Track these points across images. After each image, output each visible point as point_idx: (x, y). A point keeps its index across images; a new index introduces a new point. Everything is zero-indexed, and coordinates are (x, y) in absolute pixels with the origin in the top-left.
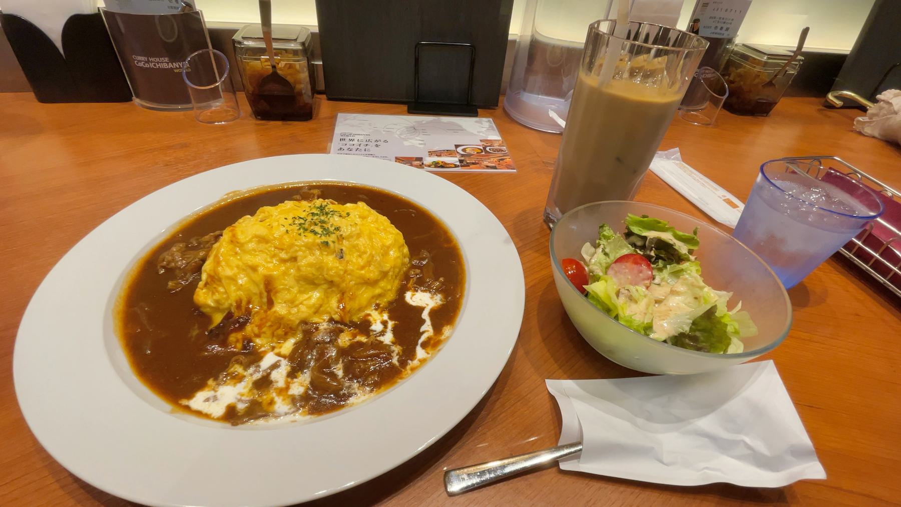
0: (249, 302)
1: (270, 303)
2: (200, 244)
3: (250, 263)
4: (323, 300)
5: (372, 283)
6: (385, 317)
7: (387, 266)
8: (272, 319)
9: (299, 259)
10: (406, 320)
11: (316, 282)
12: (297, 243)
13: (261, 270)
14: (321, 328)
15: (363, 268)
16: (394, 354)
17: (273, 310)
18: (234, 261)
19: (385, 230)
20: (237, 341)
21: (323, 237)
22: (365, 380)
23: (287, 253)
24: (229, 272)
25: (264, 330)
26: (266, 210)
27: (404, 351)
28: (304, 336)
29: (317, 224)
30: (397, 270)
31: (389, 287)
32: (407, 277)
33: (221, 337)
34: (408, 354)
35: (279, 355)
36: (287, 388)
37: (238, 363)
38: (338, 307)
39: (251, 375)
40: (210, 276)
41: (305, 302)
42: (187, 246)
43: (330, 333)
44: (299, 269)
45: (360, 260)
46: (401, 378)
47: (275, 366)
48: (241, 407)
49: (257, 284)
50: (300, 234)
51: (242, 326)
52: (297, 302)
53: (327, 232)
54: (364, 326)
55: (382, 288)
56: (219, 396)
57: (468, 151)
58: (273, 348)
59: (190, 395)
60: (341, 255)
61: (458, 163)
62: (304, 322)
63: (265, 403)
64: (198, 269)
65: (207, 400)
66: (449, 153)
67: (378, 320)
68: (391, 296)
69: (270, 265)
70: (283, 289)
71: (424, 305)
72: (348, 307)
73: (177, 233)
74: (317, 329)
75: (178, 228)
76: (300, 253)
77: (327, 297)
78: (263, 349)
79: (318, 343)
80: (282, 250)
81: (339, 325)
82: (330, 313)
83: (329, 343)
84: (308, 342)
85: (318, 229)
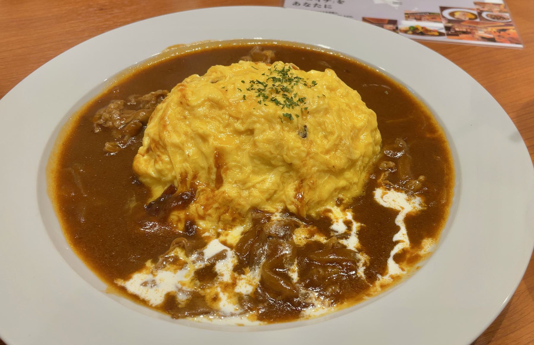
0: (195, 177)
1: (219, 181)
2: (139, 103)
3: (201, 131)
4: (279, 186)
5: (334, 172)
6: (349, 216)
7: (357, 154)
8: (220, 200)
9: (256, 132)
10: (377, 226)
11: (273, 162)
12: (255, 113)
13: (211, 140)
14: (274, 218)
15: (327, 152)
16: (360, 264)
17: (222, 189)
18: (183, 127)
19: (356, 107)
20: (179, 220)
21: (286, 109)
22: (325, 290)
23: (243, 123)
24: (175, 139)
25: (210, 211)
26: (218, 70)
27: (372, 262)
28: (254, 225)
29: (278, 92)
30: (367, 160)
31: (356, 180)
32: (376, 170)
33: (162, 214)
34: (377, 267)
35: (224, 243)
36: (234, 284)
37: (179, 246)
38: (295, 197)
39: (194, 262)
40: (153, 140)
41: (258, 186)
42: (125, 105)
43: (285, 225)
44: (255, 144)
45: (325, 142)
46: (369, 295)
47: (221, 256)
48: (182, 298)
49: (206, 158)
50: (260, 102)
51: (186, 204)
52: (250, 184)
53: (290, 103)
54: (323, 224)
55: (347, 180)
56: (158, 282)
57: (457, 15)
58: (218, 235)
59: (126, 276)
60: (304, 134)
61: (444, 31)
62: (255, 209)
63: (208, 297)
64: (139, 131)
65: (145, 284)
66: (433, 17)
67: (340, 219)
68: (356, 191)
69: (222, 136)
70: (235, 166)
71: (398, 208)
72: (307, 198)
73: (115, 88)
74: (269, 219)
75: (116, 82)
76: (258, 126)
77: (283, 183)
78: (207, 234)
79: (270, 236)
80: (238, 119)
81: (295, 218)
82: (284, 202)
83: (283, 237)
84: (258, 234)
85: (280, 98)
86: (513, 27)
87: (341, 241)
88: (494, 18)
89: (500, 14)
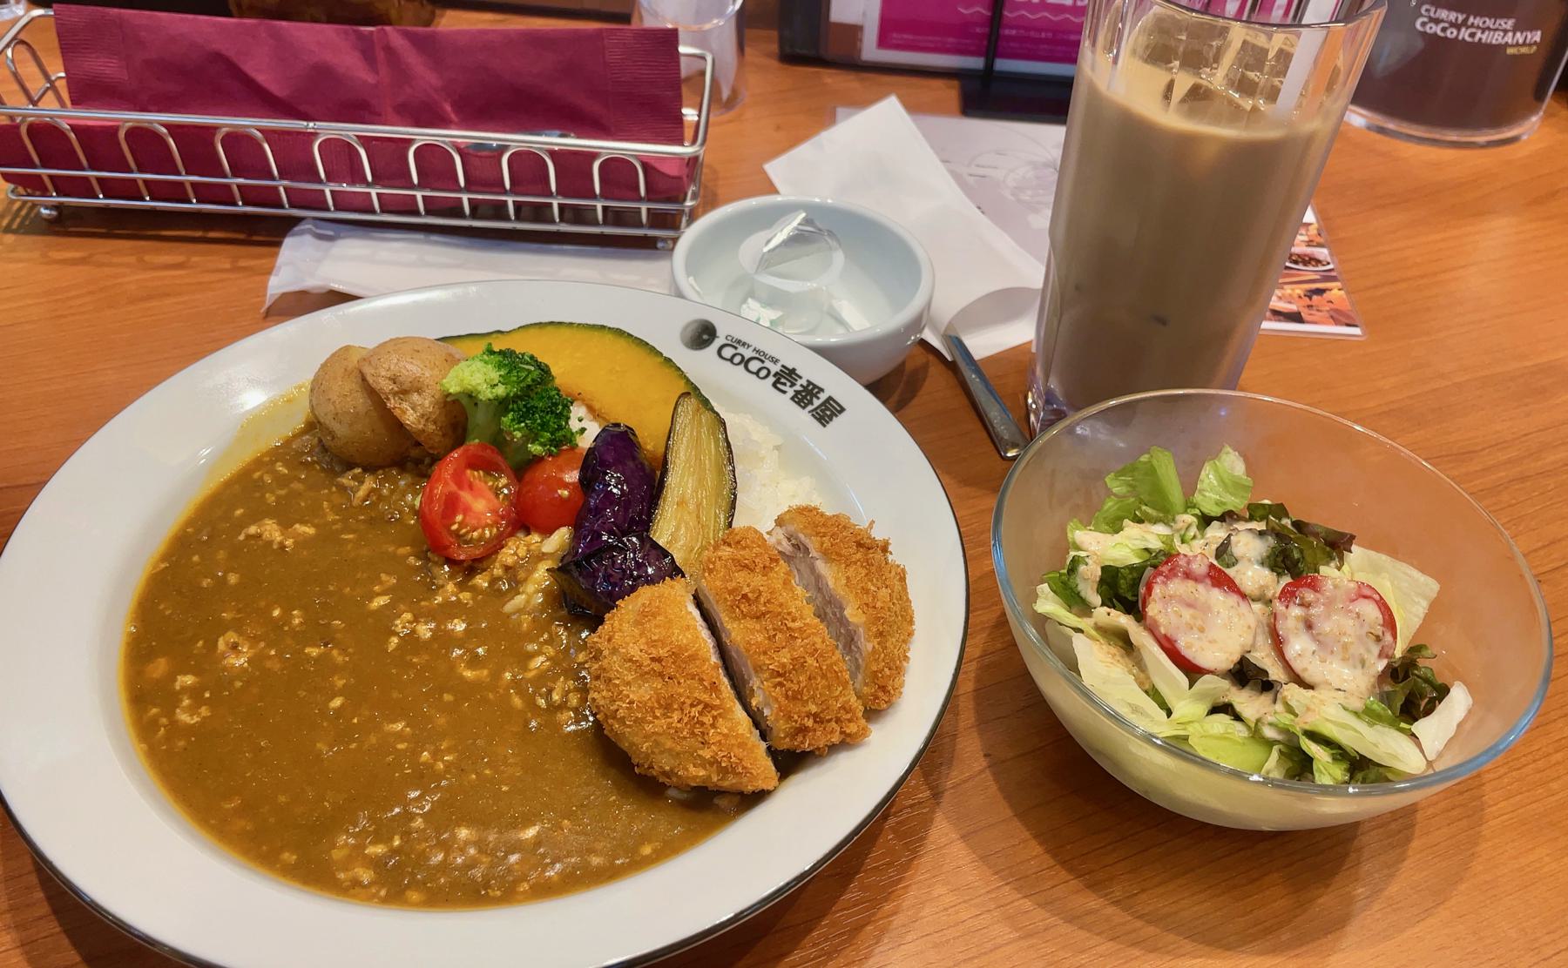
86: (1338, 284)
87: (779, 314)
88: (1296, 262)
89: (1309, 250)
